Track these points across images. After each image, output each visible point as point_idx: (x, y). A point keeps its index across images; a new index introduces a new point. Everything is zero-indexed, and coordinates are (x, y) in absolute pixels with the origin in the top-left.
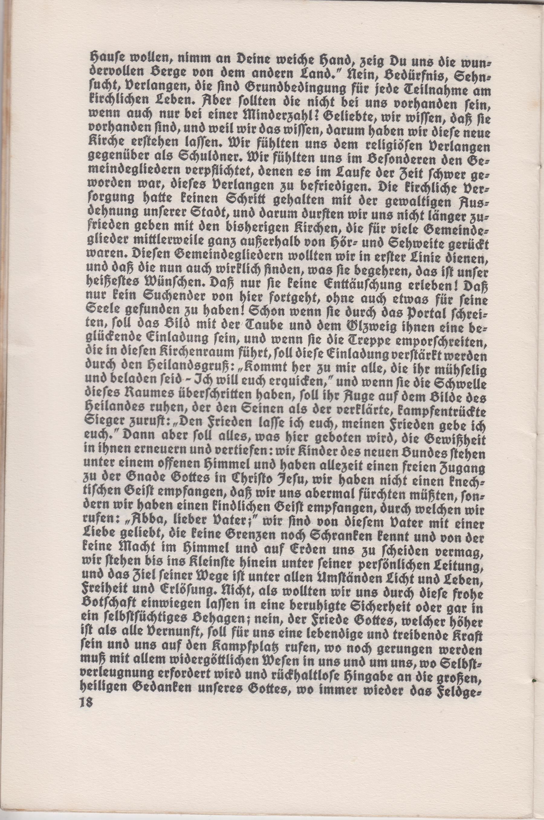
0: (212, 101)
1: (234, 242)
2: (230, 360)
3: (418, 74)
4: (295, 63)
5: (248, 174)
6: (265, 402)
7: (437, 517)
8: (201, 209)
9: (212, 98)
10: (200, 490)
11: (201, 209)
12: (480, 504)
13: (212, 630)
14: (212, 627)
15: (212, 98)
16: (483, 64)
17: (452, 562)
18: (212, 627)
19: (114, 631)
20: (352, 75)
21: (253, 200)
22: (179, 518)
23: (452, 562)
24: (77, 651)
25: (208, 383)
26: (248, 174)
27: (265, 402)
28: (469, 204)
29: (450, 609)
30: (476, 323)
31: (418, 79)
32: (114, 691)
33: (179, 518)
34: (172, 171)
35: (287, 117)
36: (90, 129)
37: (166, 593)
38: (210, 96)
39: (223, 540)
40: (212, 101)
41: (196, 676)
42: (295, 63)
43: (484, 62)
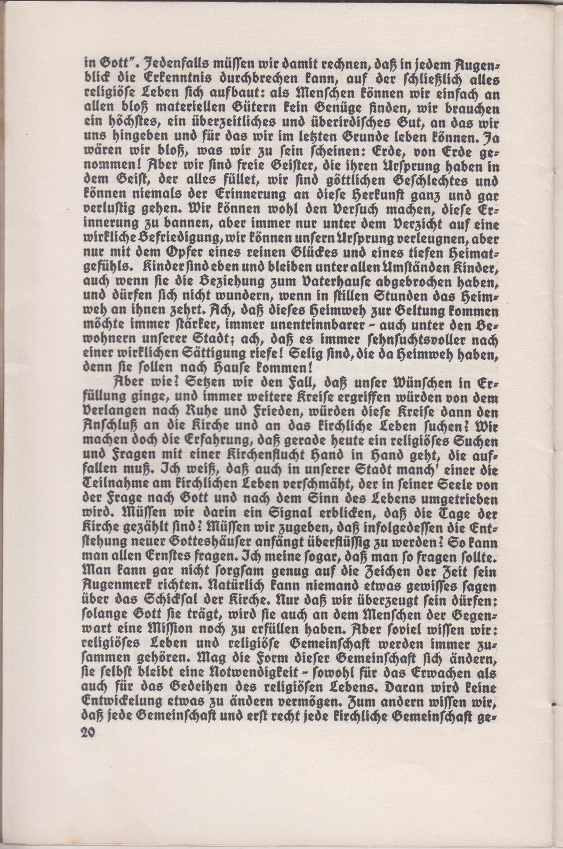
0: (124, 382)
1: (438, 197)
2: (259, 333)
3: (130, 293)
4: (383, 575)
5: (253, 183)
6: (314, 637)
7: (118, 245)
8: (203, 336)
9: (124, 380)
10: (435, 309)
11: (203, 336)
12: (494, 464)
13: (392, 627)
14: (392, 624)
15: (124, 380)
16: (491, 66)
17: (269, 393)
18: (392, 624)
19: (182, 122)
20: (213, 586)
21: (415, 240)
22: (426, 78)
23: (269, 393)
24: (78, 621)
25: (457, 83)
26: (253, 183)
27: (314, 637)
28: (93, 425)
29: (178, 513)
30: (487, 320)
31: (130, 298)
32: (485, 722)
33: (426, 78)
34: (127, 339)
35: (385, 602)
36: (85, 413)
37: (378, 155)
38: (359, 625)
39: (305, 505)
40: (124, 382)
41: (476, 662)
42: (383, 575)
43: (492, 64)
